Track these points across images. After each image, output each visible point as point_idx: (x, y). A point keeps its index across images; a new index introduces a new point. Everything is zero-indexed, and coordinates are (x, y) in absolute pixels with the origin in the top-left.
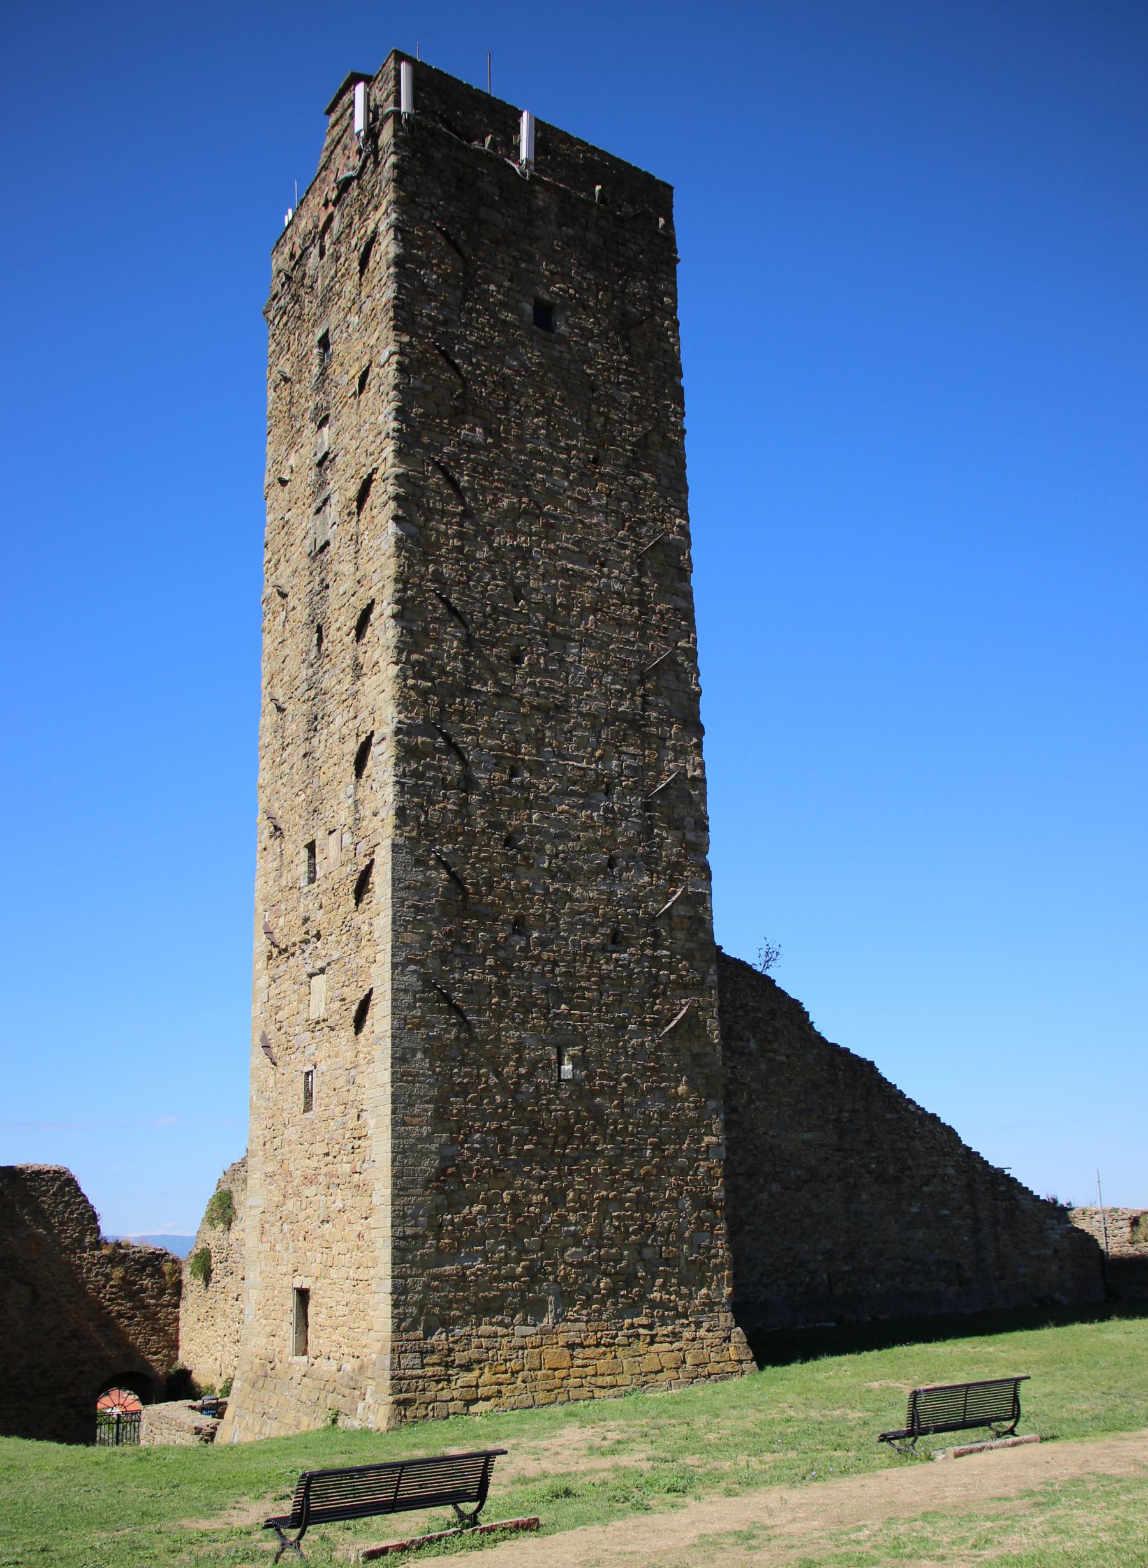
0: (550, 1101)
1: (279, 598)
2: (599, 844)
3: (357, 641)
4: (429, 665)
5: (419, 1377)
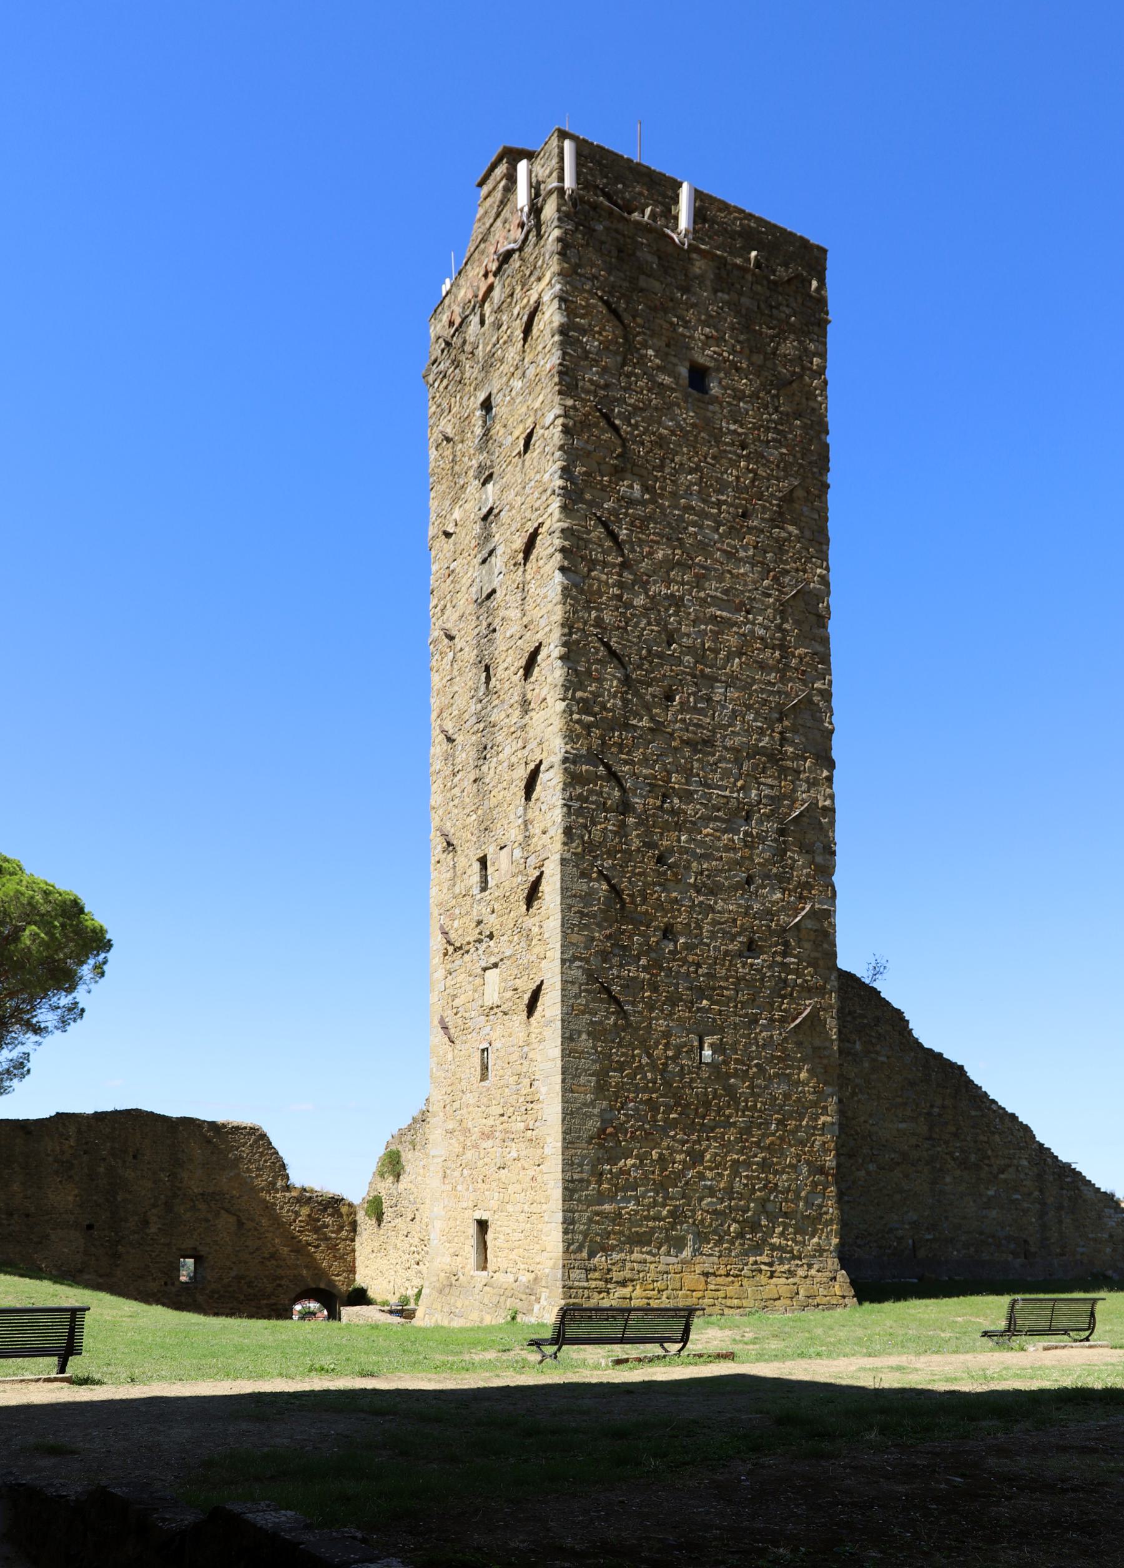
0: (692, 1080)
1: (446, 641)
2: (738, 864)
3: (525, 680)
4: (592, 702)
5: (585, 1288)
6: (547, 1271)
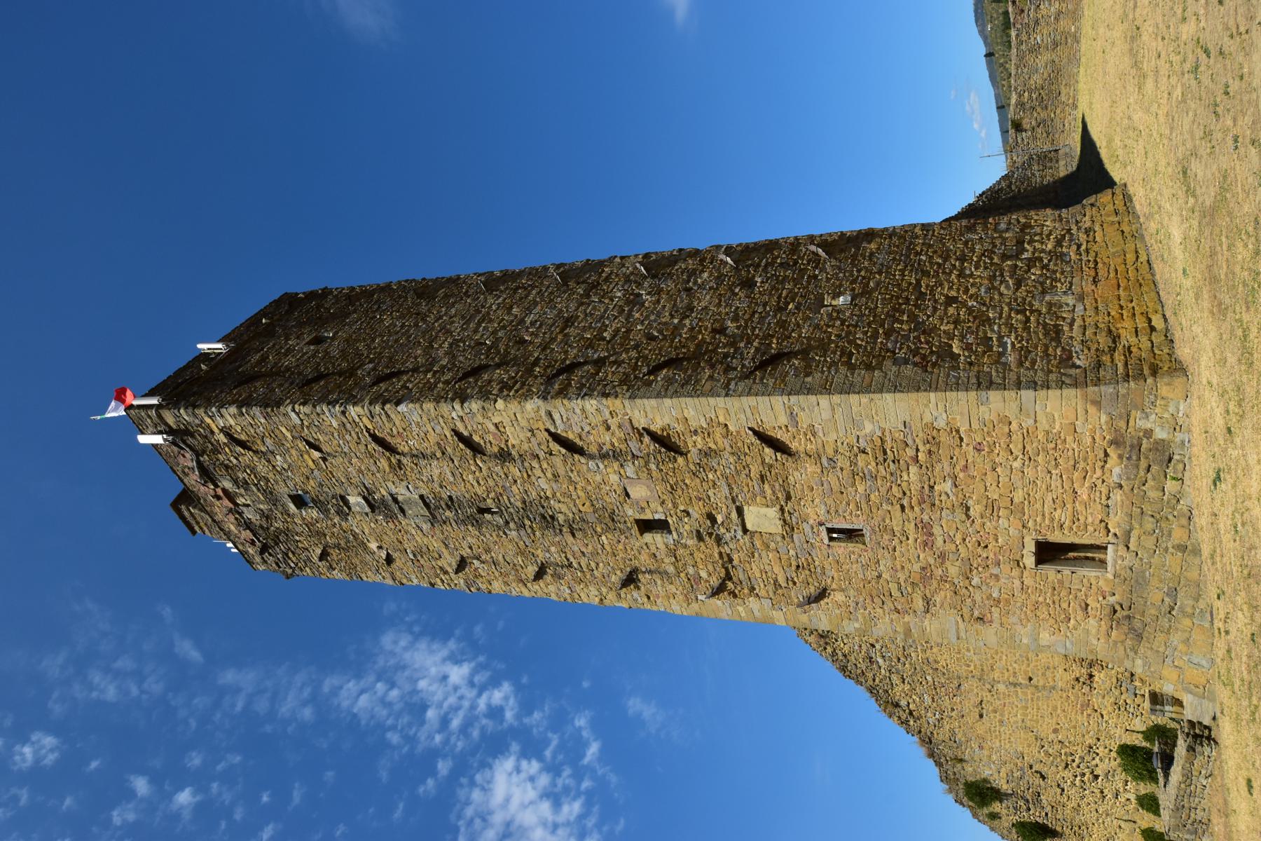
6: (1104, 418)
